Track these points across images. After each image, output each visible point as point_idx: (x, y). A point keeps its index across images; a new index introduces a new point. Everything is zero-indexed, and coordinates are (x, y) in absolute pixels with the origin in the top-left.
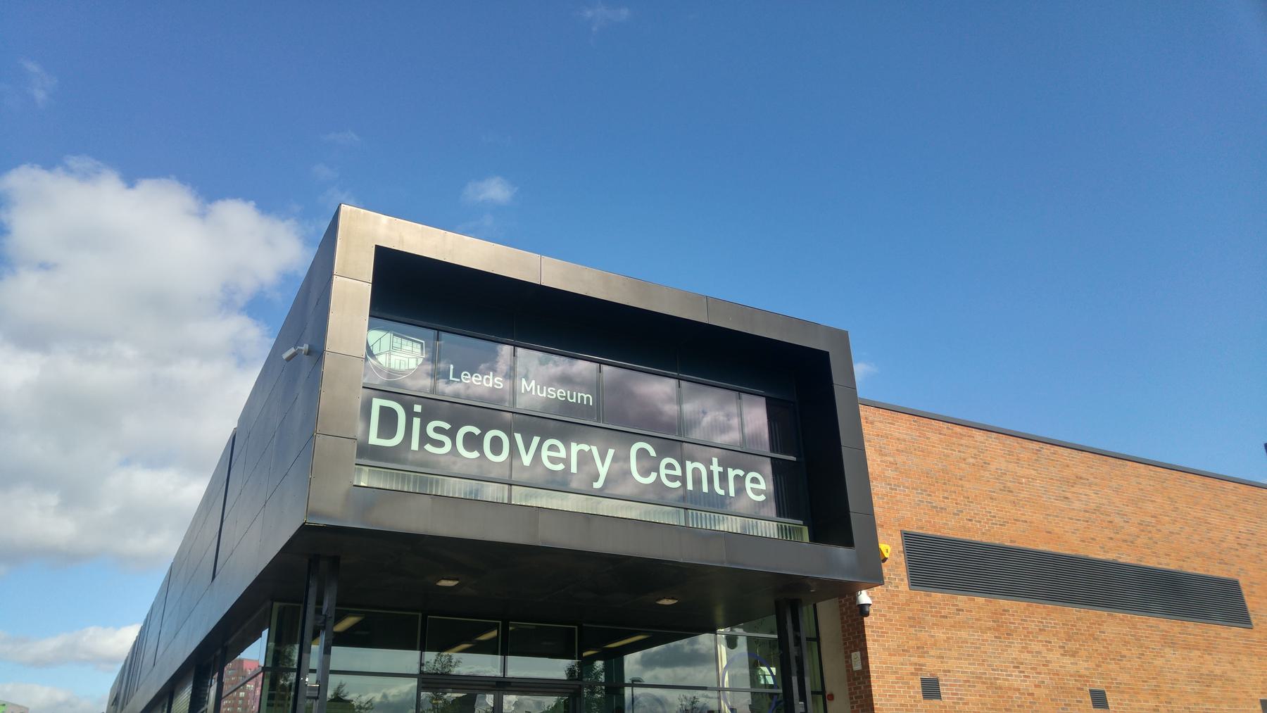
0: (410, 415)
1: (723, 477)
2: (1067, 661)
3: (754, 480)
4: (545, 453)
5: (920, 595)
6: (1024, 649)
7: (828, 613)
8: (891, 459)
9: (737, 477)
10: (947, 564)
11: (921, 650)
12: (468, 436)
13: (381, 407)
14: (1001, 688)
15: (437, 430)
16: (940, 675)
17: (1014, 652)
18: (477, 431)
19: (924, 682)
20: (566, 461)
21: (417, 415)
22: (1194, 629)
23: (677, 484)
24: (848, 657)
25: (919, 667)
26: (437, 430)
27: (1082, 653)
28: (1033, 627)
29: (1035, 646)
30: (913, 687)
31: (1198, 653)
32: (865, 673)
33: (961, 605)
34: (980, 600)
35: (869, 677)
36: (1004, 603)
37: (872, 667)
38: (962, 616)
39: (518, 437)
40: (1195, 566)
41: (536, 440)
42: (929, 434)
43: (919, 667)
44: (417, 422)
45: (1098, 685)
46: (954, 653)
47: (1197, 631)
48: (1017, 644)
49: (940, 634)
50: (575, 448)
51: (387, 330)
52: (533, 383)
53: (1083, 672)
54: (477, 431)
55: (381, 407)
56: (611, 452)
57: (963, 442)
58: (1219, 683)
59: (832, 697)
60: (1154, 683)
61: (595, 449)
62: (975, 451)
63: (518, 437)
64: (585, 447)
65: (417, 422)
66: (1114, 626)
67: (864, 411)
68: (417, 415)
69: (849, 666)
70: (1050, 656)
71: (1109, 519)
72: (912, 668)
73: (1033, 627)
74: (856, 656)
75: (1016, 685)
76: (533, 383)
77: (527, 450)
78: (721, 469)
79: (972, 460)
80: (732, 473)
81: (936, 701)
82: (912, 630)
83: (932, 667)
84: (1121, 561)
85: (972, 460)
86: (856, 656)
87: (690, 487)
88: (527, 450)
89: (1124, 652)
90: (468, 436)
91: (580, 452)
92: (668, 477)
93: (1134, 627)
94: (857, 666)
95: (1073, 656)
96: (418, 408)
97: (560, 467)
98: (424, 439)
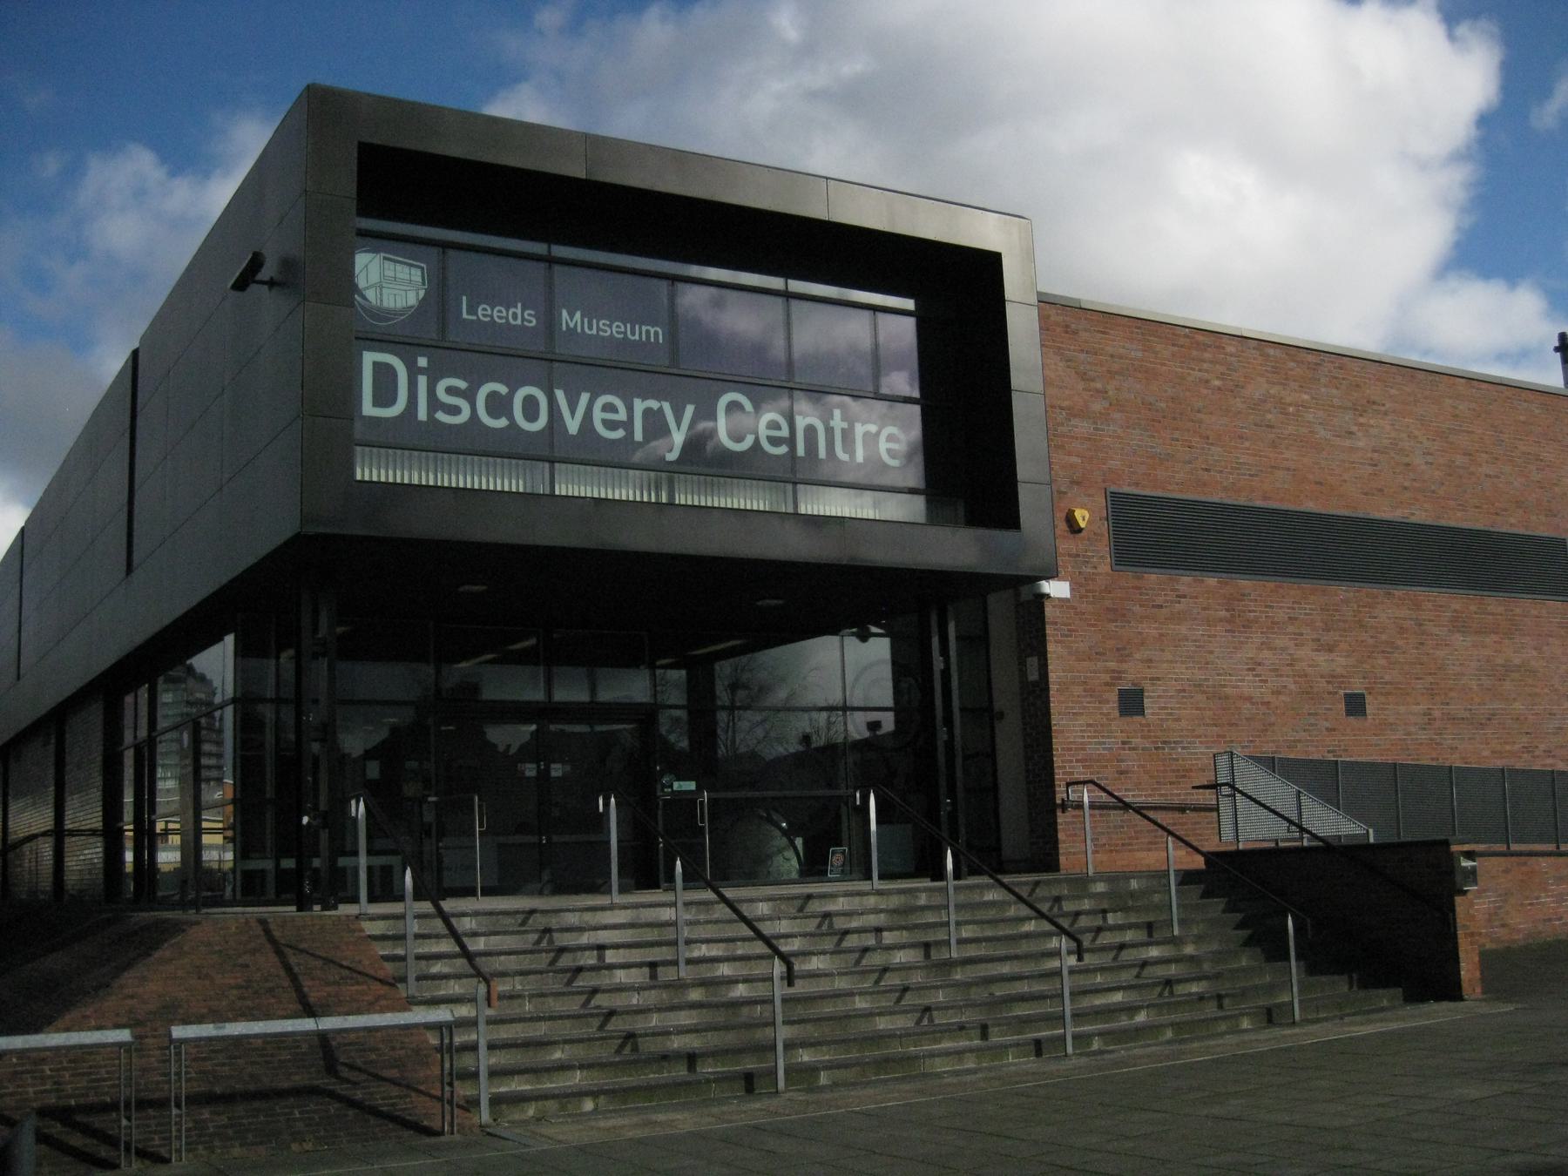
0: (413, 372)
1: (848, 436)
2: (1321, 658)
3: (890, 438)
4: (598, 416)
5: (1128, 577)
6: (1267, 645)
7: (999, 607)
8: (1099, 385)
9: (866, 434)
10: (1160, 534)
11: (1122, 654)
12: (492, 396)
13: (375, 364)
14: (1227, 697)
15: (450, 391)
16: (1147, 685)
17: (1249, 652)
18: (502, 389)
19: (1123, 694)
20: (628, 425)
21: (422, 371)
22: (1495, 605)
23: (783, 450)
24: (1022, 664)
25: (1117, 675)
26: (450, 391)
27: (1343, 646)
28: (1281, 615)
29: (1280, 642)
30: (1108, 702)
31: (1495, 637)
32: (1042, 686)
33: (1182, 588)
34: (1212, 581)
35: (1047, 689)
36: (1245, 583)
37: (1052, 677)
38: (1183, 605)
39: (560, 395)
40: (1511, 523)
41: (584, 398)
42: (1159, 347)
43: (1117, 675)
44: (422, 381)
45: (1357, 686)
46: (1168, 656)
47: (1501, 609)
48: (1257, 638)
49: (1150, 630)
50: (639, 406)
51: (376, 251)
52: (578, 315)
53: (1339, 670)
54: (502, 389)
55: (375, 364)
56: (690, 410)
57: (1207, 355)
58: (1516, 675)
59: (1001, 715)
60: (1430, 679)
61: (667, 407)
62: (1221, 369)
63: (560, 395)
64: (654, 404)
65: (422, 381)
66: (1390, 608)
67: (916, 394)
68: (422, 371)
69: (1023, 673)
70: (1300, 653)
71: (1407, 460)
72: (1106, 677)
73: (1281, 615)
74: (1033, 662)
75: (1246, 691)
76: (578, 315)
77: (573, 413)
78: (845, 425)
79: (1217, 383)
80: (860, 429)
81: (1138, 718)
82: (1112, 626)
83: (1133, 673)
84: (1413, 519)
85: (1217, 383)
86: (1033, 662)
87: (801, 451)
88: (573, 413)
89: (1400, 643)
90: (492, 396)
91: (647, 413)
92: (605, 423)
93: (1417, 606)
94: (1033, 676)
95: (1331, 651)
96: (422, 362)
97: (619, 434)
98: (434, 404)
